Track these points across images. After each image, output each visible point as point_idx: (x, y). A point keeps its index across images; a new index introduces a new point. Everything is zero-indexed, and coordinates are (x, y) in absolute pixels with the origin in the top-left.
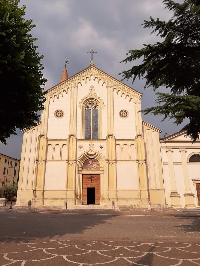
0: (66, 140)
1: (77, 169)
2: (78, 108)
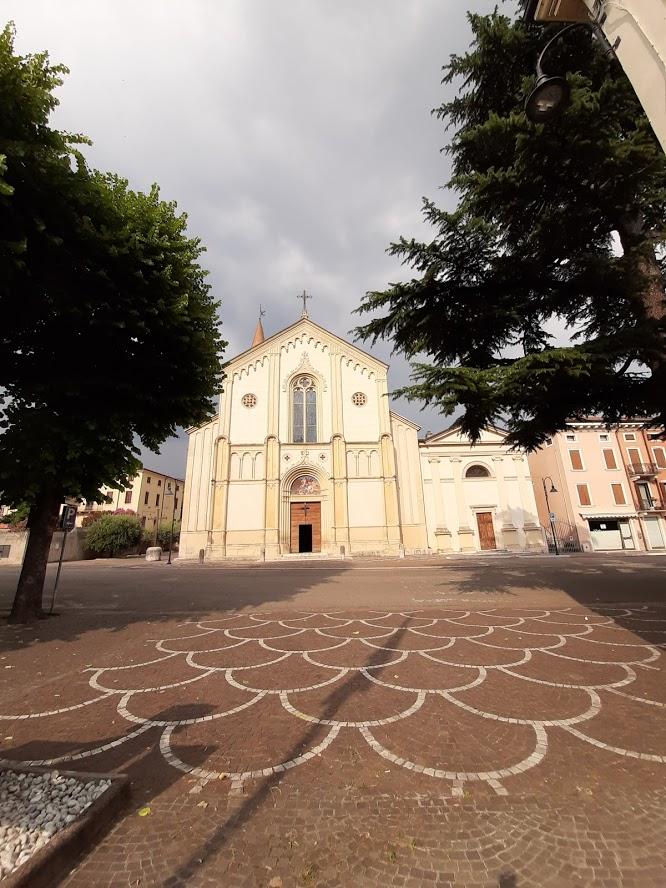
0: (376, 443)
1: (282, 494)
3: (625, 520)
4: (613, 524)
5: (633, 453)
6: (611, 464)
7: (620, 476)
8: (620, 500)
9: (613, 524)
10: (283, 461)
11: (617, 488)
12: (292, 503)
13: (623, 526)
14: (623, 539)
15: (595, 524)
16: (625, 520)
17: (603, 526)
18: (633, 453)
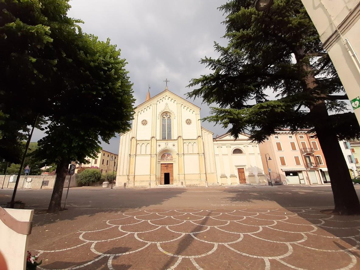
1: (157, 160)
2: (157, 118)
3: (301, 172)
4: (295, 173)
5: (303, 144)
6: (294, 148)
7: (298, 153)
8: (298, 163)
9: (295, 173)
10: (158, 146)
11: (297, 158)
12: (161, 164)
13: (299, 174)
14: (300, 180)
15: (288, 173)
16: (301, 172)
17: (291, 174)
18: (303, 144)
